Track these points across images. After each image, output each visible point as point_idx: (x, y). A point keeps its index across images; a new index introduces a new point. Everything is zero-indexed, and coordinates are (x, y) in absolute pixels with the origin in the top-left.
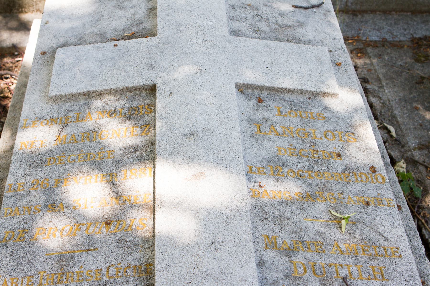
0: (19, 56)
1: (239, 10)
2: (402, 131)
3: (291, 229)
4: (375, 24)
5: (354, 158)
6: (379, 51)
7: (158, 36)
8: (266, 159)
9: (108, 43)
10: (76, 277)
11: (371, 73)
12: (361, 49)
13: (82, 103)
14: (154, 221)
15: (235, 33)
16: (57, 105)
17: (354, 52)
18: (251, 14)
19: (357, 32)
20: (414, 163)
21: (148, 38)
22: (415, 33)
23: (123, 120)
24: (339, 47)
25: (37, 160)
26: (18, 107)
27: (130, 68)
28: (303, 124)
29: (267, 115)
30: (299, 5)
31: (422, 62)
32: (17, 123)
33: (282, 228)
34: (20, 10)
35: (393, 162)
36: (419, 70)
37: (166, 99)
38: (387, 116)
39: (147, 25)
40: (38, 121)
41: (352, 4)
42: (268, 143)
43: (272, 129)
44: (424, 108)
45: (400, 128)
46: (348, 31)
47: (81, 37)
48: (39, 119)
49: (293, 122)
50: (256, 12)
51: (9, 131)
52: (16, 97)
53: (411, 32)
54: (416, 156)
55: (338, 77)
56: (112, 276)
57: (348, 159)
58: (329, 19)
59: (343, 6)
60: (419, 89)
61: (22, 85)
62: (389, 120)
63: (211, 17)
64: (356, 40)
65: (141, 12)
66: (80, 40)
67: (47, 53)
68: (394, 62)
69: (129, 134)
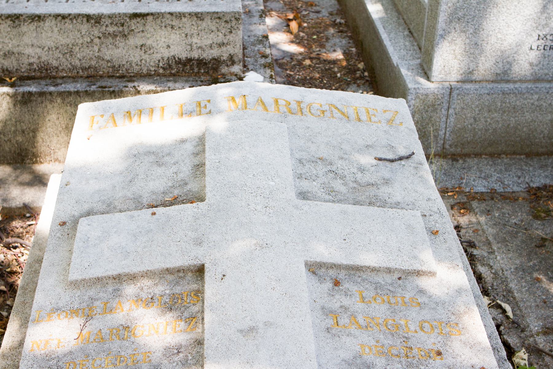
0: (32, 218)
2: (521, 310)
4: (481, 171)
5: (459, 357)
6: (487, 205)
7: (207, 201)
8: (345, 361)
9: (143, 210)
11: (478, 235)
12: (464, 204)
13: (110, 289)
15: (303, 195)
16: (79, 292)
17: (456, 207)
18: (324, 170)
19: (458, 182)
20: (538, 353)
21: (194, 204)
22: (532, 181)
23: (162, 311)
24: (435, 209)
26: (29, 289)
27: (172, 244)
28: (392, 312)
29: (346, 302)
30: (383, 156)
31: (542, 219)
32: (27, 310)
34: (34, 160)
35: (511, 352)
36: (539, 230)
37: (217, 283)
38: (501, 290)
39: (193, 186)
40: (54, 313)
41: (450, 146)
42: (348, 339)
43: (353, 321)
44: (547, 280)
45: (517, 306)
46: (446, 181)
47: (111, 203)
48: (56, 310)
49: (380, 310)
51: (17, 322)
52: (27, 276)
53: (527, 180)
54: (541, 343)
55: (434, 249)
57: (451, 359)
58: (421, 173)
59: (439, 149)
60: (540, 254)
61: (34, 260)
62: (503, 295)
63: (273, 175)
65: (186, 170)
66: (109, 206)
67: (67, 224)
68: (507, 219)
69: (170, 331)
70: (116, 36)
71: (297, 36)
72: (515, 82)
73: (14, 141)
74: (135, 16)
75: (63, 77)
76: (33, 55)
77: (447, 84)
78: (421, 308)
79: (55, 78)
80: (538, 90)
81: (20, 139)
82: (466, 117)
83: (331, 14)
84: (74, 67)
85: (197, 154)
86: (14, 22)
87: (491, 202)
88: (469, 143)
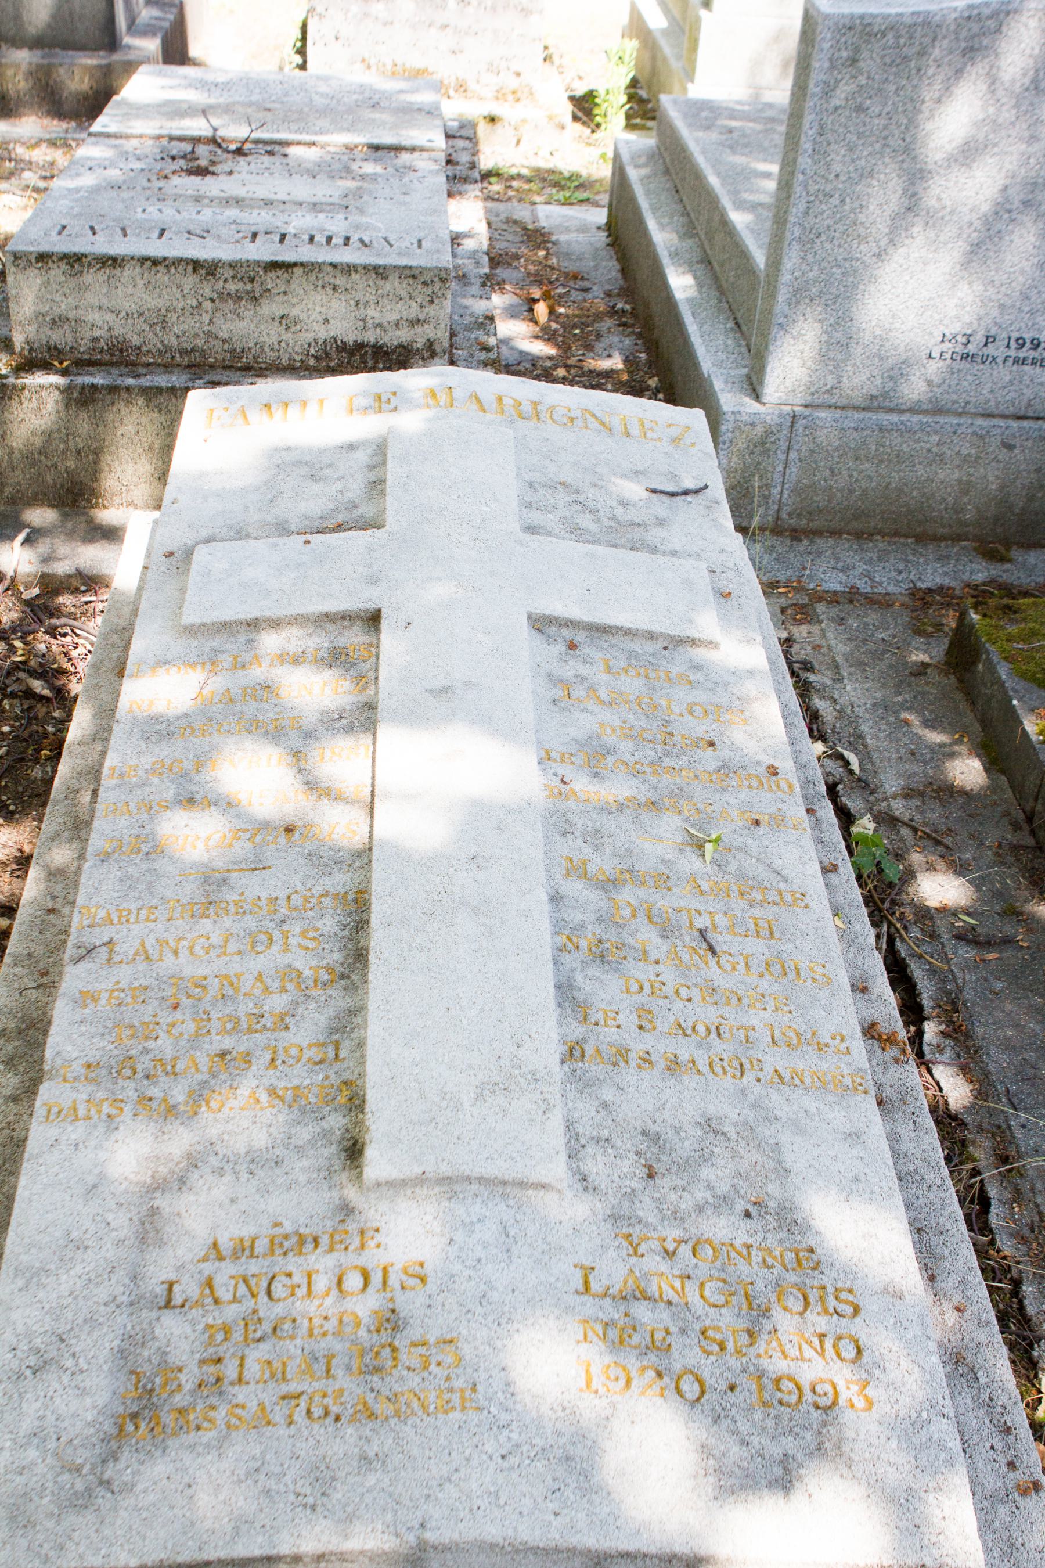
1: (542, 492)
2: (873, 764)
3: (613, 852)
4: (837, 559)
10: (232, 908)
13: (242, 639)
14: (371, 826)
15: (531, 529)
21: (369, 532)
24: (731, 565)
25: (160, 729)
29: (584, 670)
30: (659, 487)
31: (929, 635)
33: (598, 848)
39: (367, 510)
41: (789, 514)
48: (162, 663)
49: (632, 685)
50: (574, 497)
53: (912, 577)
56: (295, 909)
64: (794, 588)
65: (356, 487)
70: (240, 298)
71: (545, 329)
72: (902, 412)
73: (62, 468)
74: (274, 265)
75: (149, 365)
76: (100, 324)
77: (787, 409)
78: (692, 687)
79: (134, 364)
80: (938, 427)
81: (71, 464)
82: (818, 467)
83: (608, 294)
84: (168, 348)
85: (374, 467)
86: (73, 267)
87: (849, 607)
88: (820, 511)
